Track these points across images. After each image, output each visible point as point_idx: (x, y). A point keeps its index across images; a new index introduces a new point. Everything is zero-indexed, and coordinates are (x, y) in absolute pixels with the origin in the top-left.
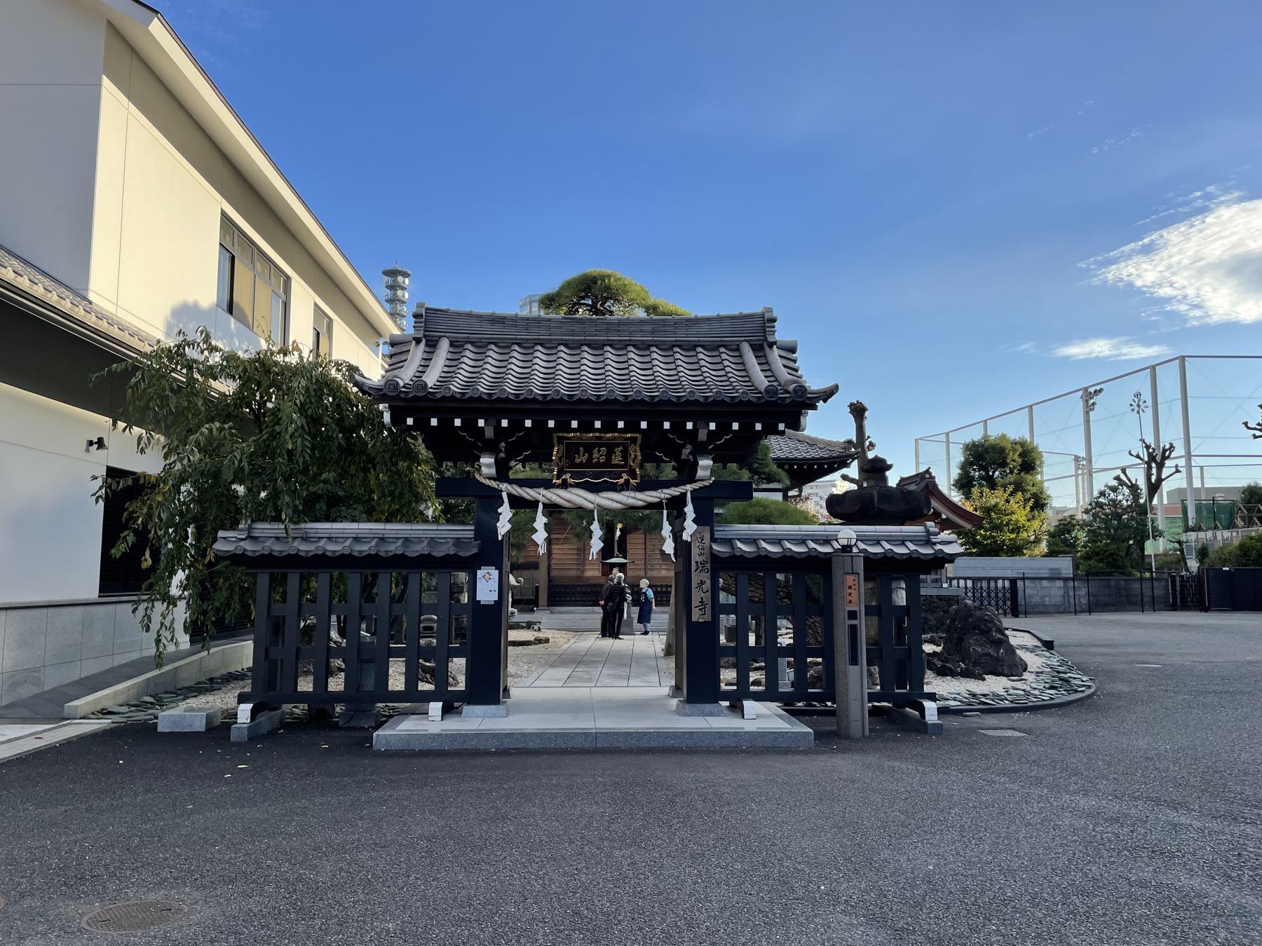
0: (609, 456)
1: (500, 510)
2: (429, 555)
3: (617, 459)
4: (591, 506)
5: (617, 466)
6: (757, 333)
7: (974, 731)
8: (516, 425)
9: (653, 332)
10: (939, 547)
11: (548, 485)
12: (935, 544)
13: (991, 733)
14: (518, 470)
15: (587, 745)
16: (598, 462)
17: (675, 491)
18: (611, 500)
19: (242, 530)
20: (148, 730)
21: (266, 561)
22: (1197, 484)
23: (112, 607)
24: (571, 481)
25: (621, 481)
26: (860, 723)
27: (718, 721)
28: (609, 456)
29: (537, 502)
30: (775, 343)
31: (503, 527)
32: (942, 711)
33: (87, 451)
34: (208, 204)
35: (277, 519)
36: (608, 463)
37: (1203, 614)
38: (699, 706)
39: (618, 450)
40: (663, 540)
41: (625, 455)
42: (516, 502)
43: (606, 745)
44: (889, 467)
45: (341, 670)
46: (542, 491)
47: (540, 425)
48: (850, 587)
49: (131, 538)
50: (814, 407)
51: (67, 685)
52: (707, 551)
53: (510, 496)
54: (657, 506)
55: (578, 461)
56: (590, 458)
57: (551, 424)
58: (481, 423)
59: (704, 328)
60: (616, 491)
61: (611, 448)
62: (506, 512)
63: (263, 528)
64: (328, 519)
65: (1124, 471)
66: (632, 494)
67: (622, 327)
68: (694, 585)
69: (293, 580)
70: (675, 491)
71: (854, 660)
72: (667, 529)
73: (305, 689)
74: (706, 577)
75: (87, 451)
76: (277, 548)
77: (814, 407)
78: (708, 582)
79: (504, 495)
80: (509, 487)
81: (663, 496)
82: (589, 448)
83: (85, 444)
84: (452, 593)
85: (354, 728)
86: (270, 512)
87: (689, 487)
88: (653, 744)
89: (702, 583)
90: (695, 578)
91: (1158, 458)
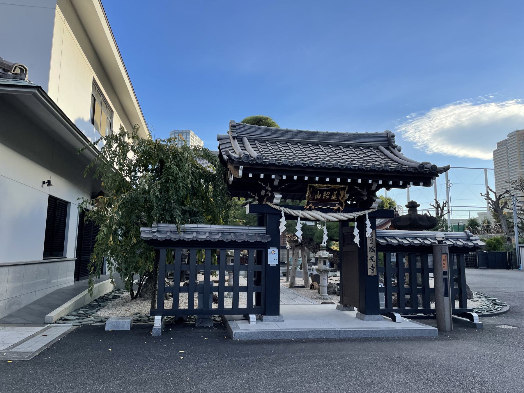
0: (330, 196)
1: (280, 220)
2: (222, 241)
3: (334, 197)
4: (323, 219)
5: (333, 201)
6: (388, 141)
7: (493, 326)
8: (290, 178)
9: (339, 139)
10: (475, 242)
11: (303, 209)
12: (472, 240)
13: (501, 327)
14: (289, 202)
15: (336, 337)
16: (325, 199)
17: (361, 213)
18: (333, 217)
19: (154, 227)
20: (99, 330)
21: (168, 243)
22: (451, 218)
23: (48, 264)
24: (313, 207)
25: (336, 208)
26: (450, 324)
27: (380, 324)
28: (330, 196)
29: (298, 217)
30: (397, 146)
31: (282, 228)
32: (482, 316)
33: (42, 186)
34: (89, 74)
35: (173, 221)
36: (330, 199)
37: (477, 270)
38: (373, 316)
39: (335, 193)
40: (354, 237)
41: (338, 195)
42: (288, 217)
43: (345, 337)
44: (419, 206)
45: (170, 296)
46: (300, 211)
47: (300, 179)
48: (444, 260)
49: (105, 230)
50: (438, 176)
51: (30, 305)
52: (374, 242)
53: (285, 213)
54: (353, 220)
55: (316, 197)
56: (322, 196)
57: (306, 178)
58: (273, 177)
59: (362, 138)
60: (333, 212)
61: (332, 191)
62: (283, 221)
63: (163, 226)
64: (192, 222)
65: (428, 212)
66: (342, 214)
67: (325, 136)
68: (369, 258)
69: (163, 252)
70: (361, 213)
71: (446, 295)
72: (356, 232)
73: (183, 308)
74: (374, 254)
75: (42, 186)
76: (173, 237)
77: (438, 176)
78: (375, 257)
79: (283, 213)
80: (285, 209)
81: (356, 215)
82: (322, 191)
83: (42, 183)
84: (182, 258)
85: (203, 327)
86: (168, 218)
87: (367, 212)
88: (367, 336)
89: (372, 257)
90: (369, 255)
91: (441, 206)
